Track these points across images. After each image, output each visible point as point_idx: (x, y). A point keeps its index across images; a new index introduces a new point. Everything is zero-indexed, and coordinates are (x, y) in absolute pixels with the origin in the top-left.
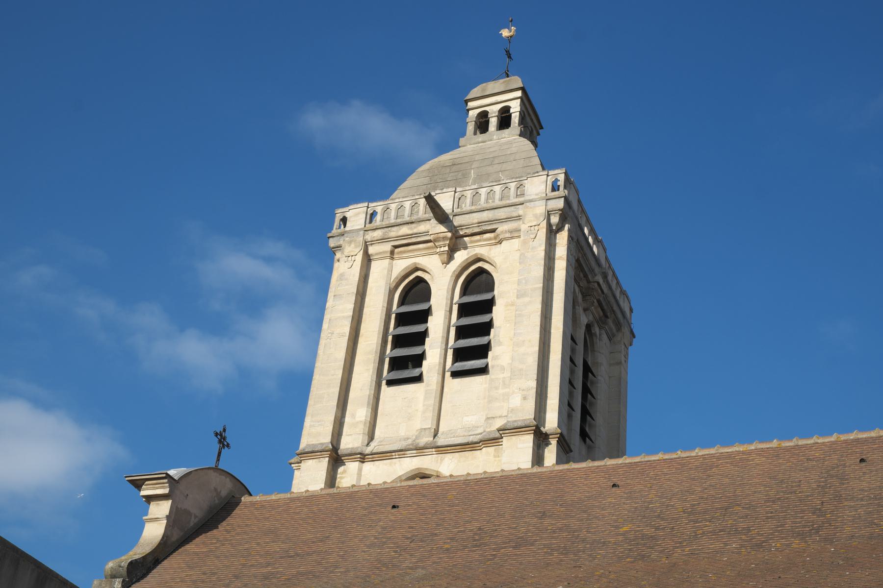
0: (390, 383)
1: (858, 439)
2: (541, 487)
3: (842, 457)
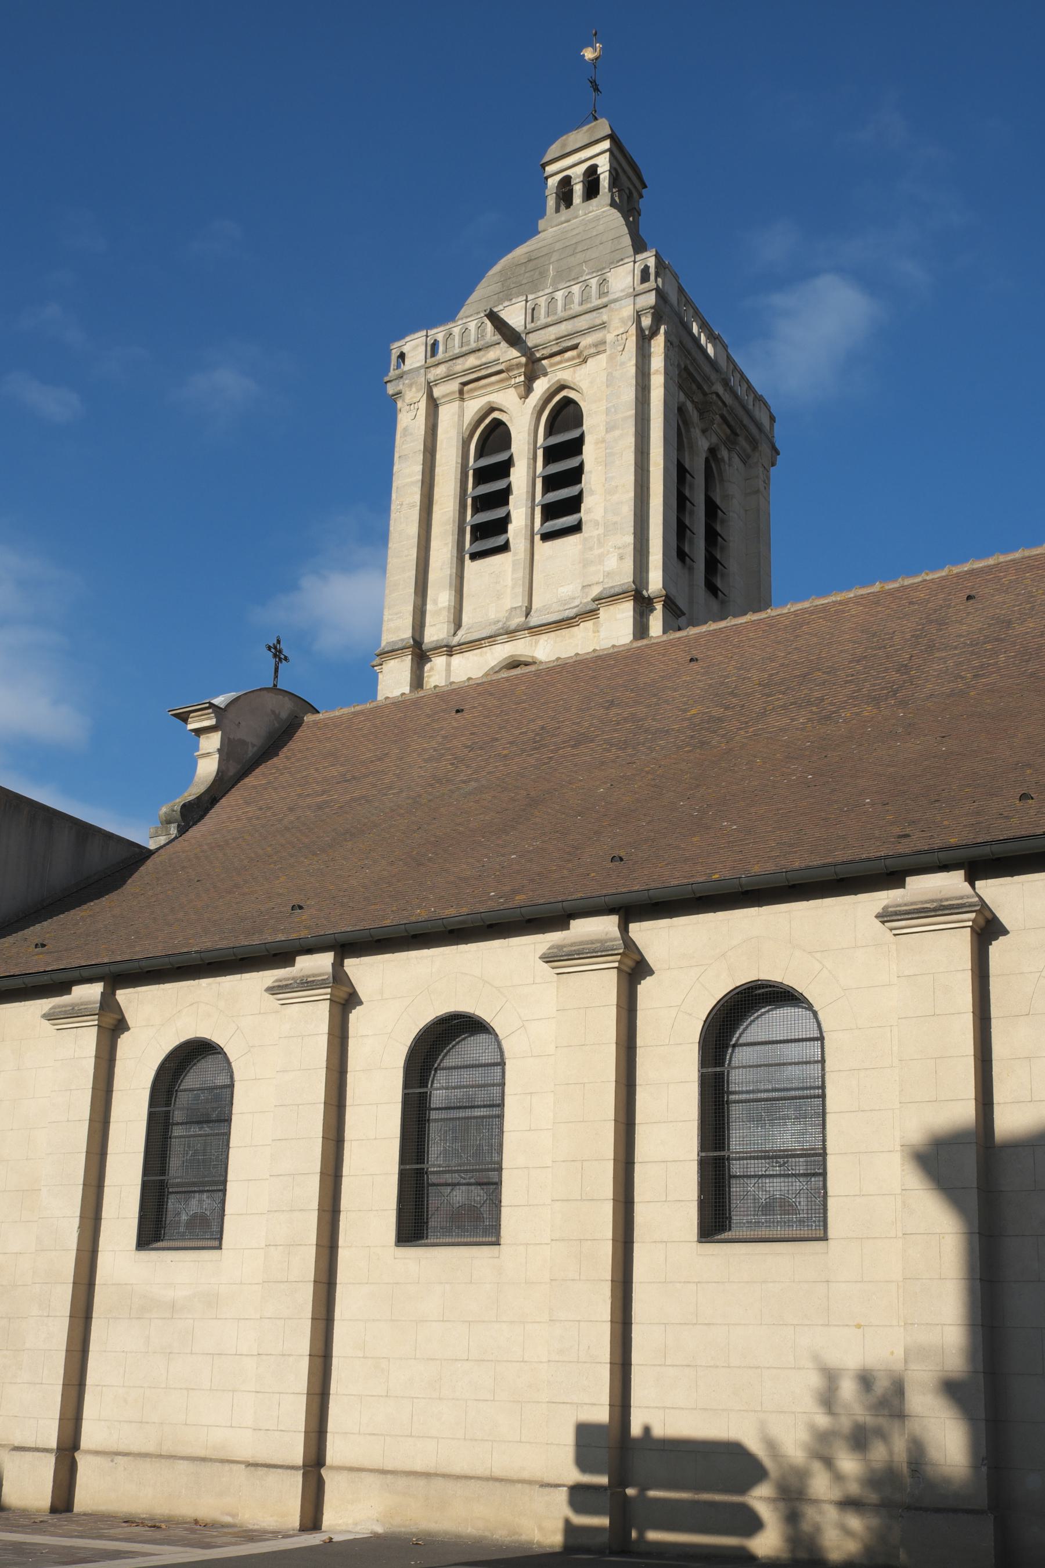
0: (474, 556)
1: (973, 570)
2: (615, 670)
3: (950, 596)
